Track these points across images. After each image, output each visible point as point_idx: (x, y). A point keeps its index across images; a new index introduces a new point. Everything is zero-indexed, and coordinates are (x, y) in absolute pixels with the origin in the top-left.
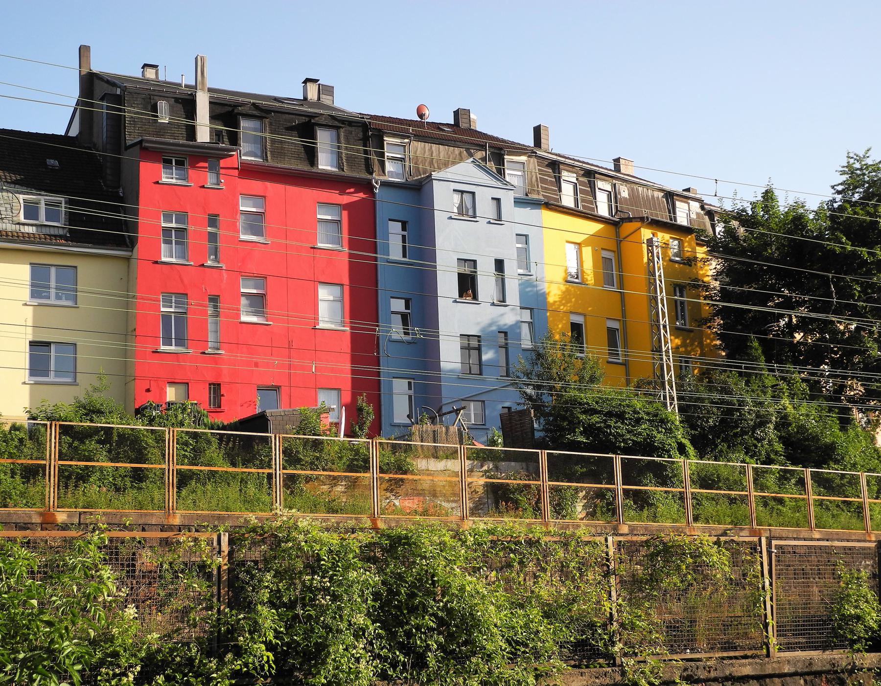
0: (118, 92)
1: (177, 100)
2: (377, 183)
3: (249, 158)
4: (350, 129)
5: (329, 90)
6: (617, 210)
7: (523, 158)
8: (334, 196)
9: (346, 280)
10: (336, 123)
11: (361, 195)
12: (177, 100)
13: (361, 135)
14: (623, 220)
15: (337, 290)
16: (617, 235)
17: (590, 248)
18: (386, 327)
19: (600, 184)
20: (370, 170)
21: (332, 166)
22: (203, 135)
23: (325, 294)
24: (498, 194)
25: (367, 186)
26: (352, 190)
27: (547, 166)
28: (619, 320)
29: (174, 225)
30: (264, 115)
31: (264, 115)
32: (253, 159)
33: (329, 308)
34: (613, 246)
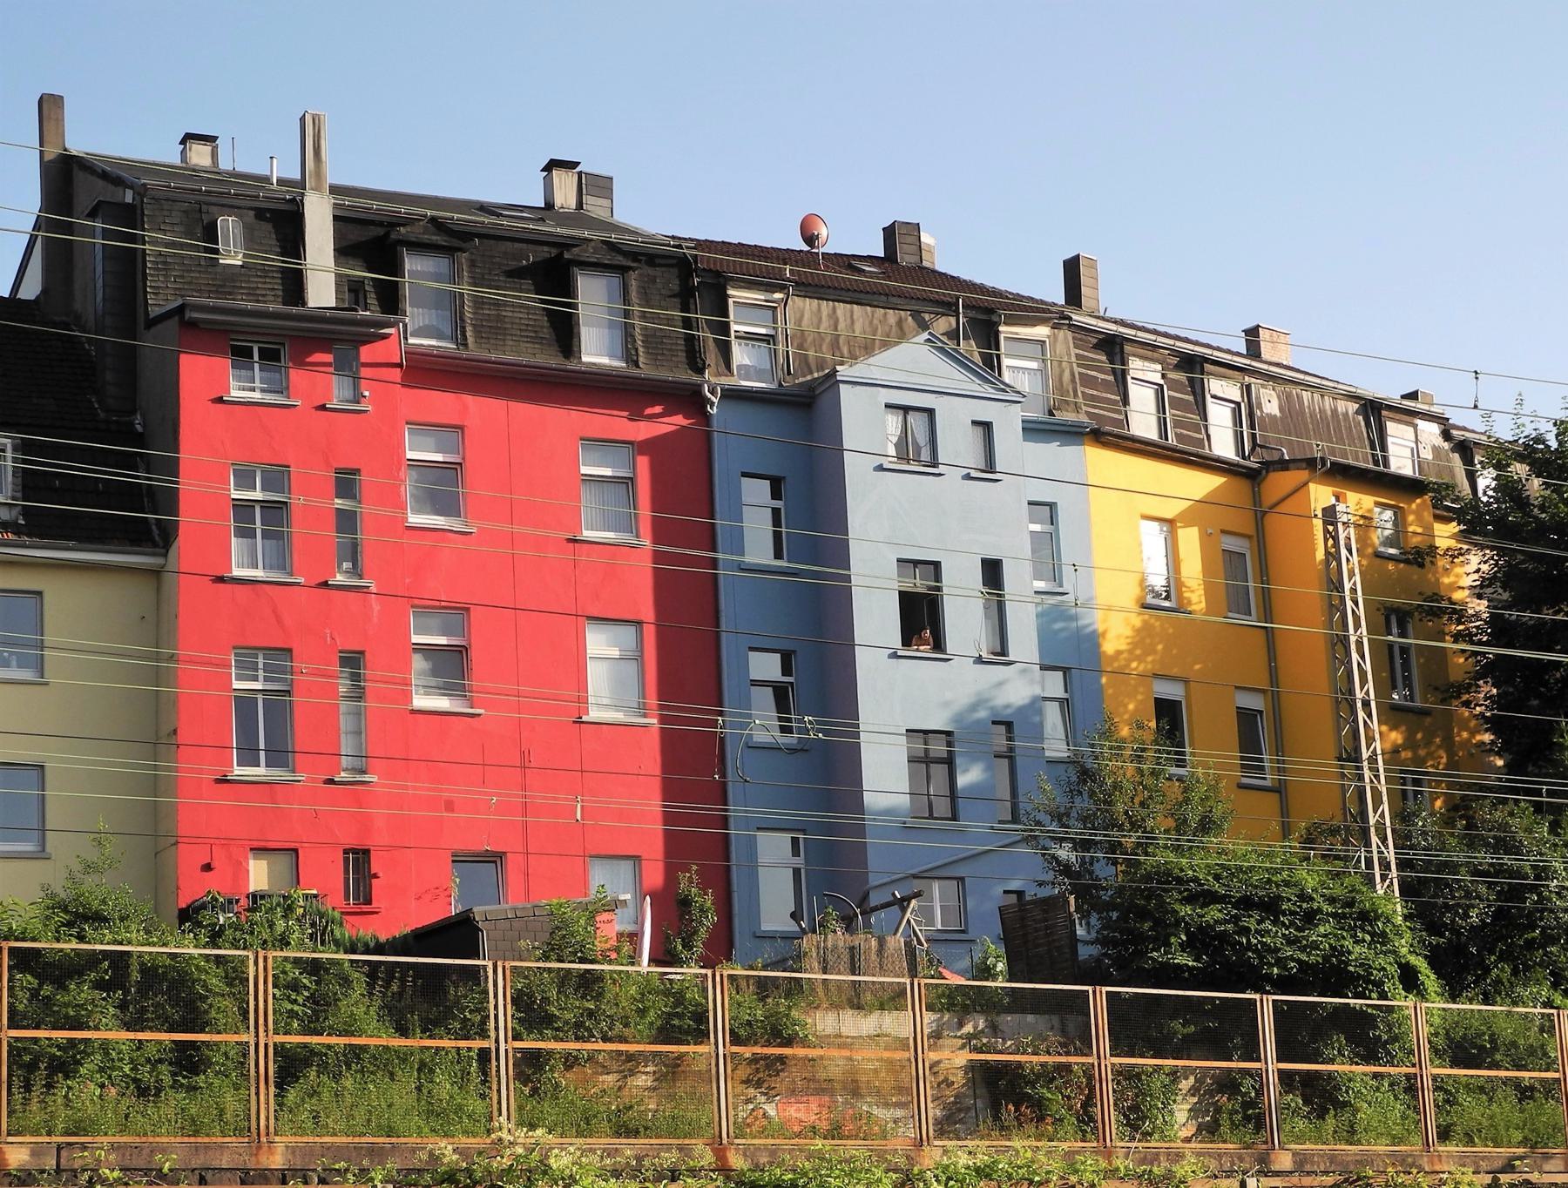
0: (129, 197)
1: (260, 214)
2: (713, 392)
4: (651, 271)
5: (600, 185)
7: (1042, 331)
9: (648, 613)
10: (620, 260)
11: (679, 420)
12: (260, 214)
13: (675, 285)
14: (1268, 466)
15: (629, 633)
16: (1256, 499)
19: (1215, 386)
21: (611, 356)
22: (322, 291)
23: (601, 645)
24: (985, 412)
25: (692, 401)
26: (658, 409)
29: (258, 495)
30: (456, 243)
31: (456, 243)
32: (433, 342)
33: (610, 674)
34: (1246, 524)
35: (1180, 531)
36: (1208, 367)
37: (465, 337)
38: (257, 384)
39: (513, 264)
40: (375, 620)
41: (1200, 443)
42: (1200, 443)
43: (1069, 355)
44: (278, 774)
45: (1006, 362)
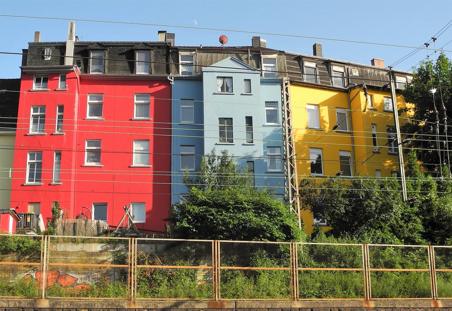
1: (56, 47)
2: (171, 79)
3: (94, 73)
4: (158, 50)
5: (172, 36)
6: (349, 84)
7: (275, 56)
8: (146, 89)
10: (148, 47)
11: (163, 87)
12: (56, 47)
13: (165, 53)
14: (350, 89)
15: (146, 144)
16: (349, 98)
17: (326, 107)
18: (68, 171)
19: (335, 68)
20: (168, 72)
21: (145, 72)
23: (137, 147)
24: (248, 77)
25: (166, 82)
26: (157, 84)
27: (294, 59)
28: (350, 151)
29: (39, 114)
30: (104, 48)
31: (104, 48)
32: (97, 73)
33: (140, 155)
34: (345, 105)
35: (321, 108)
36: (332, 63)
37: (104, 71)
38: (41, 86)
39: (121, 52)
40: (65, 143)
41: (329, 84)
42: (329, 84)
43: (284, 62)
44: (38, 183)
45: (263, 65)
